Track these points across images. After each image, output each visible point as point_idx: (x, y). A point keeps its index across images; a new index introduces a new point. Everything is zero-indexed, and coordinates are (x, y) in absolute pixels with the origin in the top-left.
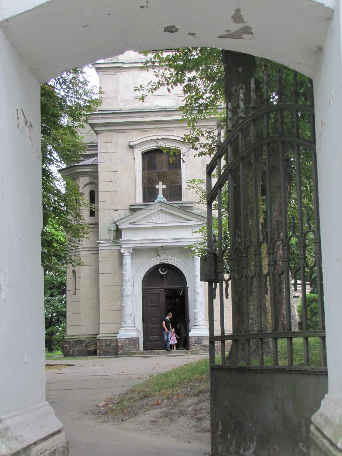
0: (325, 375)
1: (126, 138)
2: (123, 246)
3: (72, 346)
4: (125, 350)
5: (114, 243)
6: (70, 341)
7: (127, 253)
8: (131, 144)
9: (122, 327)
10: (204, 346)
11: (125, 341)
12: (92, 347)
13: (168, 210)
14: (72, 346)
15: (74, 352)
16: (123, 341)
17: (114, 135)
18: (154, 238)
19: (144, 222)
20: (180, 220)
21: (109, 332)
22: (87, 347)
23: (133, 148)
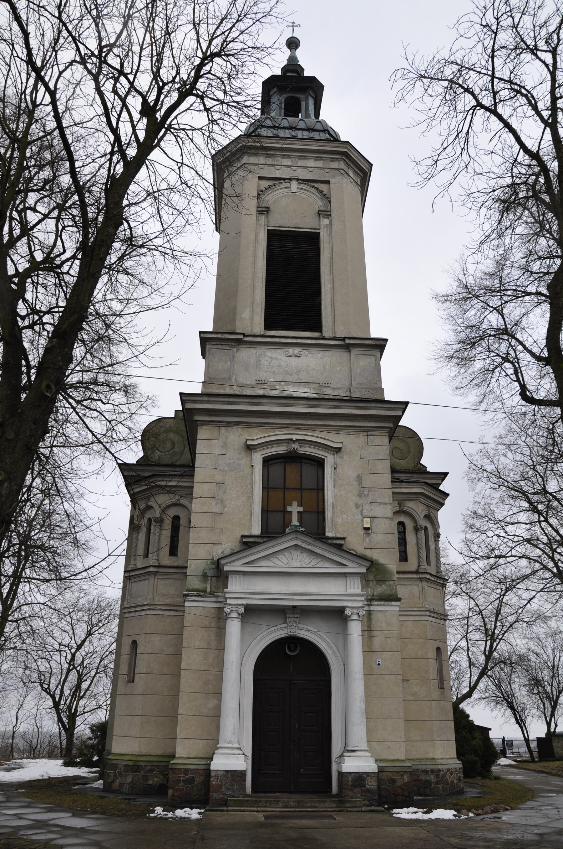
0: (381, 760)
1: (241, 435)
2: (229, 601)
3: (120, 773)
4: (225, 794)
5: (211, 597)
6: (116, 764)
7: (234, 615)
8: (249, 443)
9: (218, 748)
10: (369, 791)
11: (224, 776)
12: (155, 779)
13: (308, 547)
14: (120, 773)
15: (121, 785)
16: (221, 776)
17: (223, 430)
18: (283, 592)
19: (264, 563)
20: (327, 565)
21: (192, 756)
22: (146, 778)
23: (251, 450)
